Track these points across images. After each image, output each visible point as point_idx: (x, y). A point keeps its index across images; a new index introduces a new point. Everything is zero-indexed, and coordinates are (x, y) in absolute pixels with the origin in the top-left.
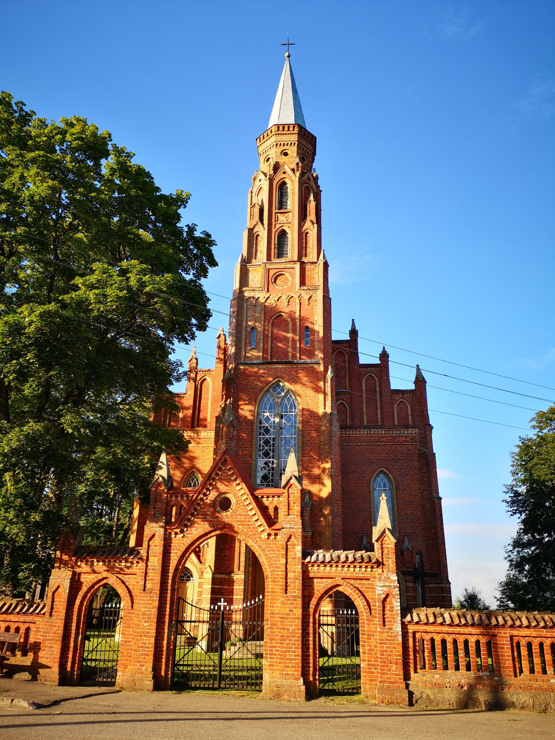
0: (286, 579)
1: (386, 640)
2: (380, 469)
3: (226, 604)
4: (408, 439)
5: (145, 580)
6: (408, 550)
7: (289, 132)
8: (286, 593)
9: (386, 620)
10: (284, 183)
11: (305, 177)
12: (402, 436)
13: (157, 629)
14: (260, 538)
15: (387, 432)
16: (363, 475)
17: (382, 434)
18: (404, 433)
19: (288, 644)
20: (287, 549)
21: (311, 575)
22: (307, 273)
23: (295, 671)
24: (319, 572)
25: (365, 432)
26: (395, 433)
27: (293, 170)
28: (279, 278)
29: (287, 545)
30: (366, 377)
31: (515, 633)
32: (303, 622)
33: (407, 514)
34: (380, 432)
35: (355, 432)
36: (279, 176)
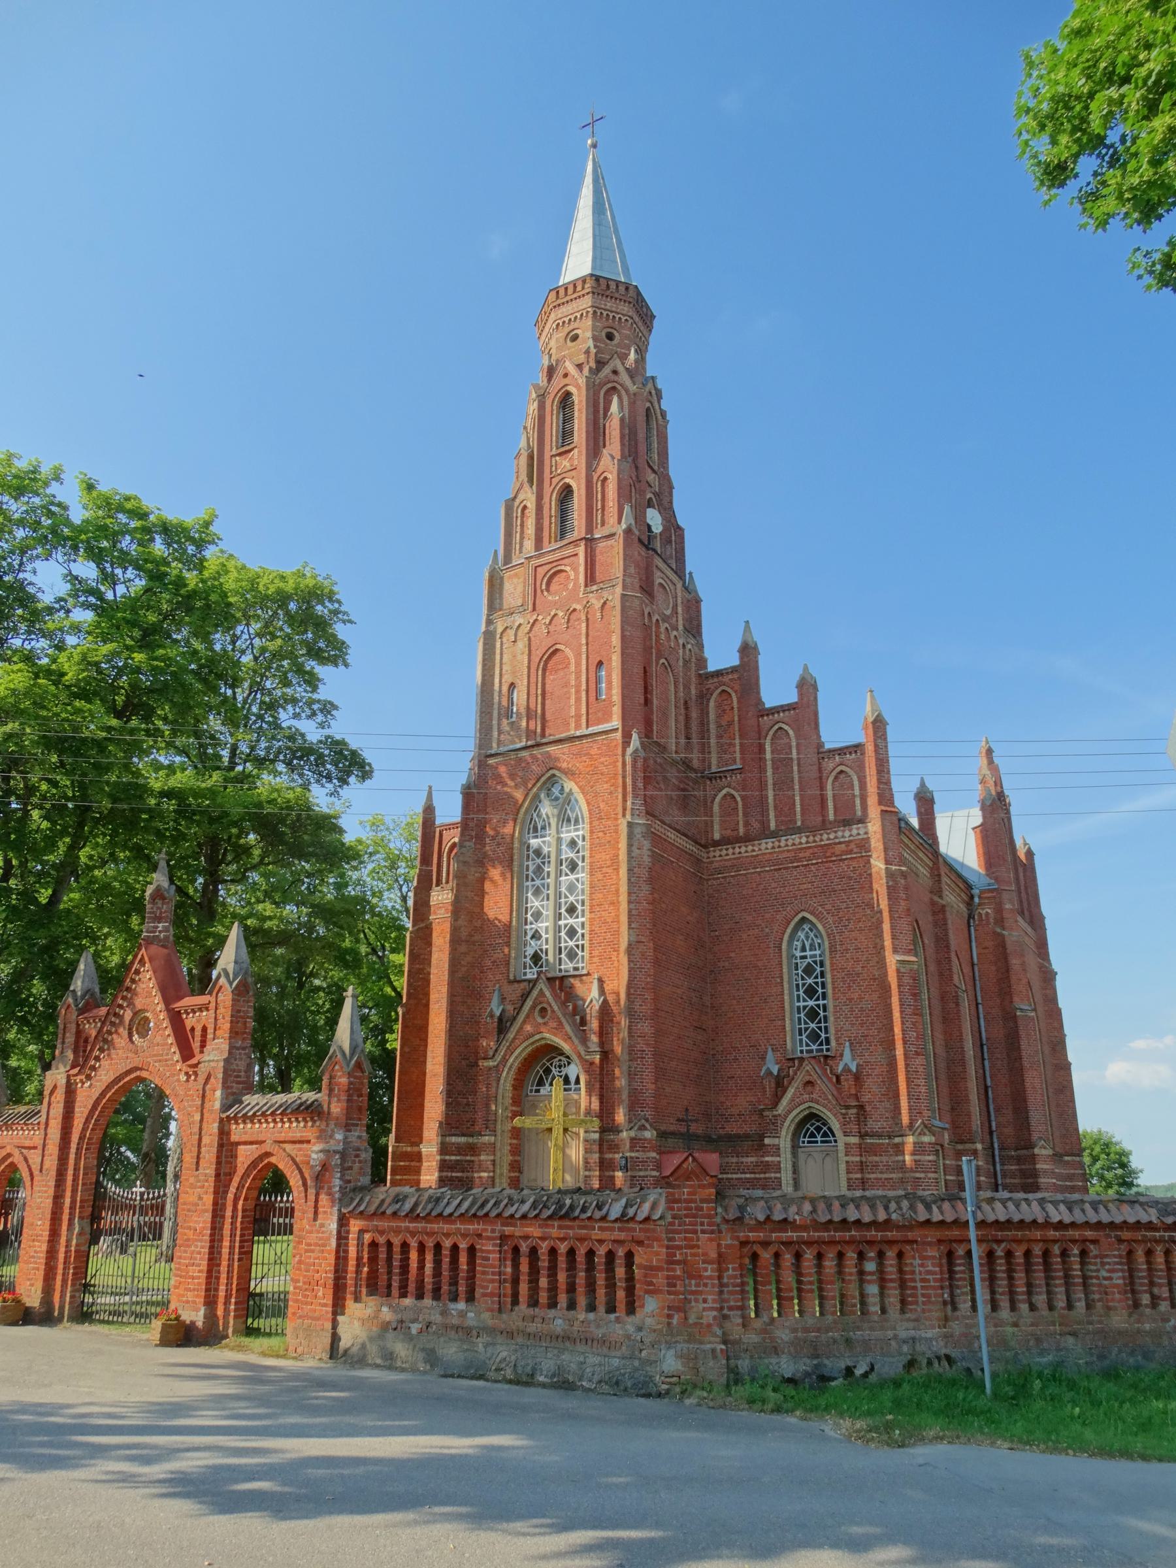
0: (199, 1146)
1: (316, 1245)
2: (800, 916)
3: (143, 1189)
4: (852, 846)
5: (43, 1156)
6: (850, 1071)
7: (568, 298)
8: (197, 1170)
9: (321, 1210)
10: (568, 395)
11: (607, 370)
12: (840, 843)
13: (51, 1230)
14: (179, 1080)
15: (811, 839)
16: (767, 930)
17: (801, 843)
18: (843, 837)
19: (192, 1253)
20: (203, 1096)
21: (234, 1138)
22: (599, 558)
23: (197, 1296)
24: (246, 1133)
25: (770, 845)
26: (826, 838)
27: (579, 366)
28: (556, 579)
29: (204, 1090)
30: (771, 733)
31: (508, 1230)
32: (214, 1216)
33: (850, 1000)
34: (797, 841)
35: (750, 848)
36: (558, 382)
